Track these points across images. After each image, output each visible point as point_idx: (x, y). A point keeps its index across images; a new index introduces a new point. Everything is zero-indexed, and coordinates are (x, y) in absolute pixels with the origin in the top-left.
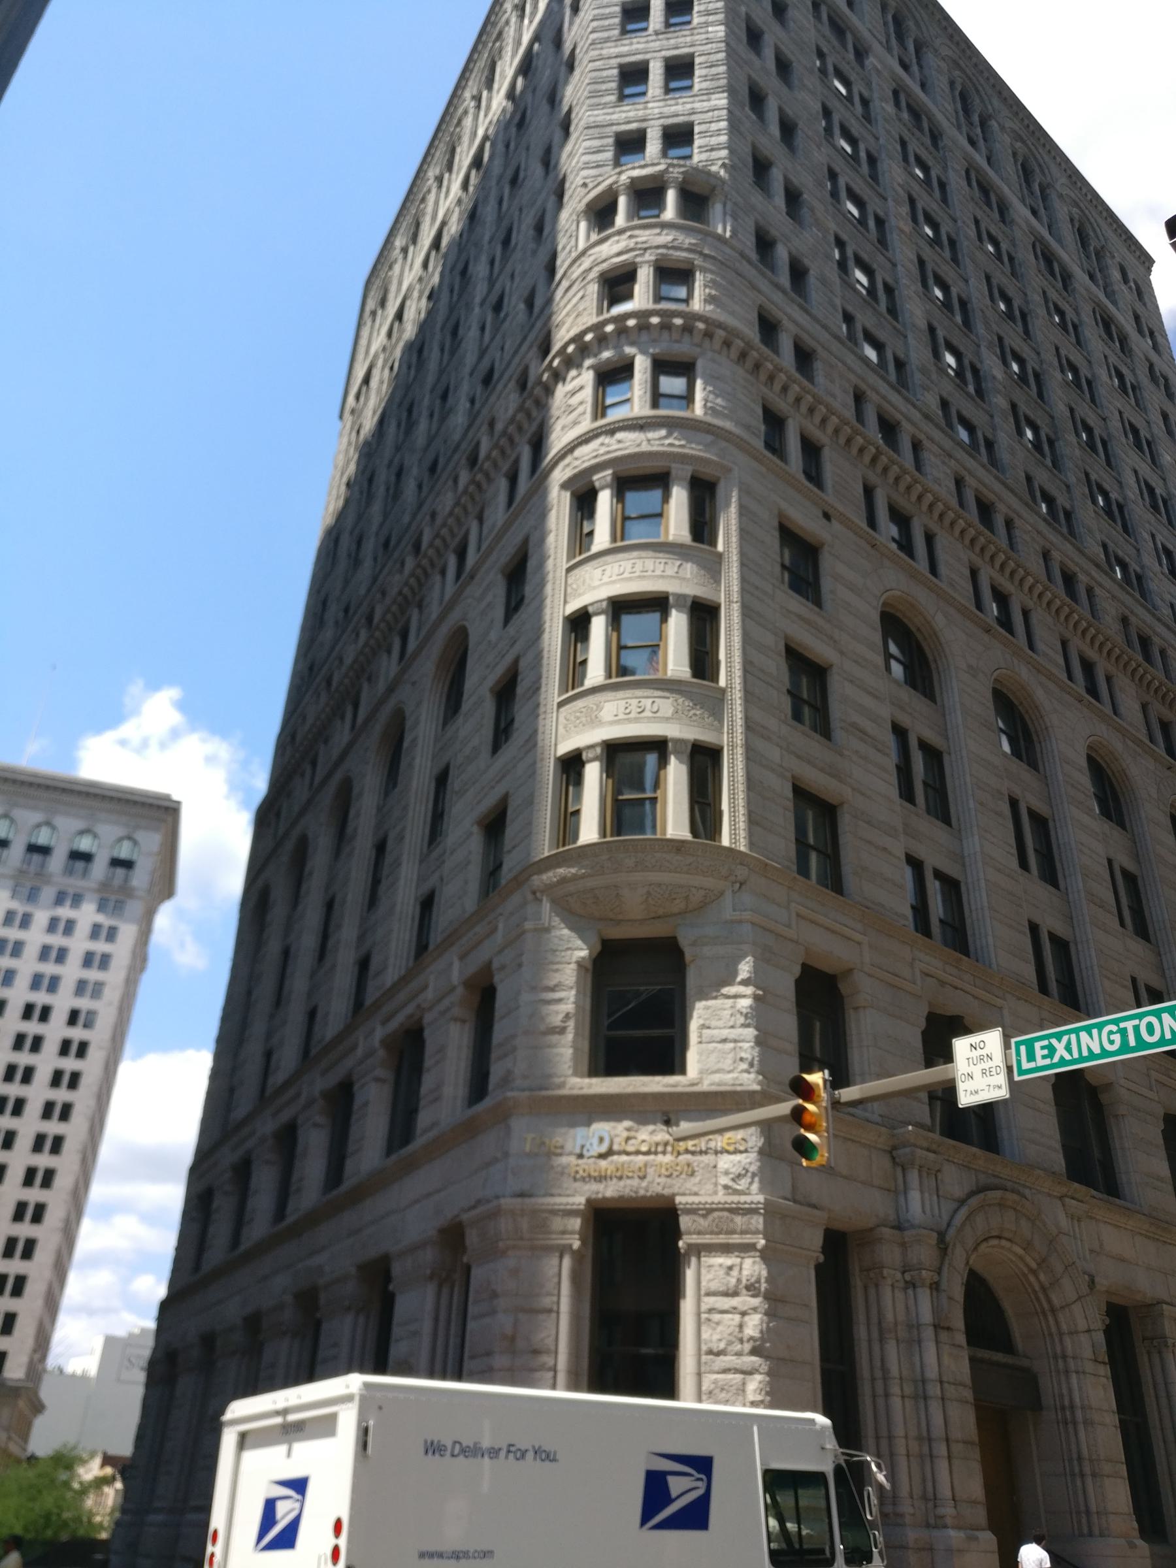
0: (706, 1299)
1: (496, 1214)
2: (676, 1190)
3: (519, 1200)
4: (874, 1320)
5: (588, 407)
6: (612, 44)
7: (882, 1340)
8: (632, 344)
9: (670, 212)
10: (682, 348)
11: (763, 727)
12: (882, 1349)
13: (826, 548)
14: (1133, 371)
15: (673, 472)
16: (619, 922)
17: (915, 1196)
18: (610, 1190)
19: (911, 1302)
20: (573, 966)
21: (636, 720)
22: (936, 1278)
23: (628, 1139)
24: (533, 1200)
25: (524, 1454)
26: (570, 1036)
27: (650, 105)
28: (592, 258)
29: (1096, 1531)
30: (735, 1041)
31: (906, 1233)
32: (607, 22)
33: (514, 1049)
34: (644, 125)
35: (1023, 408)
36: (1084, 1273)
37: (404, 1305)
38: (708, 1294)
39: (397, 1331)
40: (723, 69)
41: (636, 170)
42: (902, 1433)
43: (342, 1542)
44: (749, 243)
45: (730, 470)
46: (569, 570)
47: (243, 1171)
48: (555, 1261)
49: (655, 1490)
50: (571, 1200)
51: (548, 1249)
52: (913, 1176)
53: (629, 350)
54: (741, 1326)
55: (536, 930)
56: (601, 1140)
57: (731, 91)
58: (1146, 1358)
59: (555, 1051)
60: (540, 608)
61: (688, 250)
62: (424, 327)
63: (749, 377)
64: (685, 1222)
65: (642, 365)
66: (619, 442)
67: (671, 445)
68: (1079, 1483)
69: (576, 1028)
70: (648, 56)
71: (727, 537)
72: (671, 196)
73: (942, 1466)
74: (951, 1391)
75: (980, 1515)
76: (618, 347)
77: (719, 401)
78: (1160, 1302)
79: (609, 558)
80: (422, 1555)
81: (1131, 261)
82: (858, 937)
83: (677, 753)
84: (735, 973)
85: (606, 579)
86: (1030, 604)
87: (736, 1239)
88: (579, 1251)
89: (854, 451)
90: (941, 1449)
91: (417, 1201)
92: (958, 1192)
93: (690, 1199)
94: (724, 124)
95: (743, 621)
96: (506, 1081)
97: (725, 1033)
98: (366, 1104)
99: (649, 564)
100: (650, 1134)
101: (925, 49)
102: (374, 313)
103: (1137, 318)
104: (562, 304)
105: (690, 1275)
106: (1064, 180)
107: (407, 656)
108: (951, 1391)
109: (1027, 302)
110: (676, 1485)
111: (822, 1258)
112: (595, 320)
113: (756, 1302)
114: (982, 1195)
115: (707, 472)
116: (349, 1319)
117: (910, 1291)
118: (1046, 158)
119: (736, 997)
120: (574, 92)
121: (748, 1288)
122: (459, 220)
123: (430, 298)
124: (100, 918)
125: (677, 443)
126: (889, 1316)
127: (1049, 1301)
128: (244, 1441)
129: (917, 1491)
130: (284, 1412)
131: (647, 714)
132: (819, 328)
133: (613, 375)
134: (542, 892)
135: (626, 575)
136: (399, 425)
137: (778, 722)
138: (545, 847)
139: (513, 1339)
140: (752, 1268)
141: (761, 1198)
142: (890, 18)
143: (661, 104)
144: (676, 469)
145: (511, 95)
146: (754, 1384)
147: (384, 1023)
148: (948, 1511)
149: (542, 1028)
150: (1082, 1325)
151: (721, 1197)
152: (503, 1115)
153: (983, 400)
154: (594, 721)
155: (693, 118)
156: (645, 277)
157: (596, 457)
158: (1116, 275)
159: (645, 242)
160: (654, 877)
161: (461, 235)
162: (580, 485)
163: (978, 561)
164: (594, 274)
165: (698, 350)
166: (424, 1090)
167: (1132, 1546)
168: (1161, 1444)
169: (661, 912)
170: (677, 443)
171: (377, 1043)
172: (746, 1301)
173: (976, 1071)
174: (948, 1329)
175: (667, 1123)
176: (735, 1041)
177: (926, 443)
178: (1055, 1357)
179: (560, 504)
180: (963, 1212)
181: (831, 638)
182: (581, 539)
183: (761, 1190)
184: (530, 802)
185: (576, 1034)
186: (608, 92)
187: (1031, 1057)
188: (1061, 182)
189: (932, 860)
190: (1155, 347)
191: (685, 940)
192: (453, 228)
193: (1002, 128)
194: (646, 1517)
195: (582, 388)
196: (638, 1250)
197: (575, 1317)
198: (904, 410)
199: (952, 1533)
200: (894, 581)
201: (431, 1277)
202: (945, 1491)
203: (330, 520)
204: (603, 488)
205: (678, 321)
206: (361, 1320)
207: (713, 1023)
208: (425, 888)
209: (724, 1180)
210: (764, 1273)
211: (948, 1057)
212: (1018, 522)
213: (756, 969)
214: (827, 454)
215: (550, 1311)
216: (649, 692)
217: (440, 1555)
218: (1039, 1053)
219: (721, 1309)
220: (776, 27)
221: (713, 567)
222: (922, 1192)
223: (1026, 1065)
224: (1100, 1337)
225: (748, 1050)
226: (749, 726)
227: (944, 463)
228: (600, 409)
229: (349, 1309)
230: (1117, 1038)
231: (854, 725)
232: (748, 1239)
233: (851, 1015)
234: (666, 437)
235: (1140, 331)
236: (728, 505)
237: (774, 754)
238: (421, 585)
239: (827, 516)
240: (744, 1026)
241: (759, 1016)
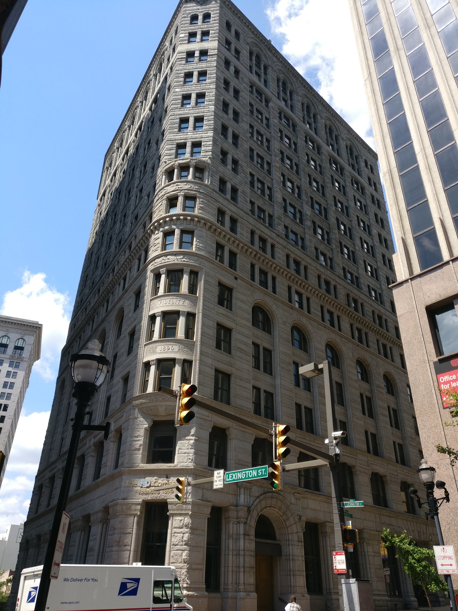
0: (174, 529)
1: (117, 504)
3: (123, 500)
5: (160, 245)
6: (178, 110)
7: (228, 539)
8: (174, 225)
9: (190, 177)
10: (190, 227)
11: (206, 353)
12: (228, 541)
13: (235, 289)
14: (365, 200)
15: (184, 270)
16: (158, 416)
17: (242, 496)
18: (149, 497)
19: (238, 527)
20: (143, 430)
21: (166, 353)
22: (246, 521)
23: (155, 482)
24: (127, 500)
25: (89, 580)
26: (141, 451)
27: (188, 134)
28: (165, 191)
29: (292, 592)
30: (188, 453)
31: (238, 507)
32: (177, 102)
33: (125, 455)
34: (186, 141)
35: (318, 223)
36: (298, 515)
37: (93, 529)
38: (174, 528)
39: (91, 538)
40: (212, 122)
41: (181, 161)
42: (231, 565)
44: (217, 184)
45: (202, 268)
46: (151, 300)
47: (52, 479)
48: (132, 518)
49: (123, 587)
50: (138, 500)
51: (131, 515)
52: (242, 490)
53: (174, 227)
54: (183, 537)
55: (133, 418)
56: (148, 482)
57: (215, 130)
58: (321, 539)
59: (137, 456)
60: (142, 312)
61: (195, 191)
62: (121, 184)
63: (212, 235)
64: (170, 507)
65: (177, 232)
66: (168, 259)
67: (184, 261)
68: (289, 578)
69: (143, 449)
70: (189, 115)
71: (200, 292)
72: (191, 170)
73: (242, 574)
74: (247, 553)
75: (253, 588)
76: (170, 225)
77: (201, 245)
79: (163, 298)
80: (62, 603)
81: (369, 157)
85: (161, 305)
86: (310, 296)
87: (183, 512)
88: (140, 515)
89: (248, 253)
90: (242, 570)
91: (99, 497)
92: (257, 494)
93: (171, 500)
94: (211, 143)
95: (202, 319)
96: (122, 464)
97: (186, 451)
98: (88, 463)
99: (175, 300)
101: (294, 93)
102: (107, 168)
103: (369, 179)
104: (156, 205)
105: (170, 522)
106: (346, 132)
107: (108, 311)
108: (247, 553)
109: (324, 182)
110: (129, 585)
111: (210, 517)
112: (164, 215)
113: (187, 530)
114: (265, 495)
115: (195, 269)
116: (79, 533)
117: (238, 524)
118: (339, 125)
119: (190, 440)
120: (166, 124)
121: (185, 526)
122: (133, 148)
123: (124, 173)
124: (10, 369)
125: (186, 260)
126: (231, 532)
127: (286, 524)
128: (25, 578)
129: (234, 582)
130: (34, 572)
131: (170, 350)
132: (240, 210)
133: (168, 234)
135: (167, 304)
136: (112, 219)
137: (212, 351)
138: (137, 392)
139: (119, 542)
140: (187, 520)
141: (191, 500)
142: (281, 84)
143: (192, 133)
144: (185, 268)
145: (150, 109)
147: (94, 438)
148: (242, 587)
149: (133, 449)
150: (295, 531)
152: (120, 475)
153: (302, 224)
154: (154, 352)
155: (202, 139)
156: (180, 199)
157: (161, 263)
158: (363, 164)
159: (181, 188)
161: (134, 154)
162: (156, 272)
163: (291, 284)
164: (165, 197)
165: (195, 227)
166: (103, 462)
167: (303, 596)
168: (323, 565)
169: (170, 413)
170: (186, 260)
171: (92, 445)
174: (248, 535)
176: (188, 453)
177: (277, 245)
178: (286, 541)
179: (150, 277)
180: (258, 500)
181: (233, 320)
184: (134, 376)
185: (143, 451)
186: (175, 128)
187: (228, 478)
188: (344, 134)
189: (263, 387)
190: (376, 190)
192: (131, 151)
193: (321, 118)
195: (159, 238)
196: (156, 514)
197: (137, 534)
198: (269, 234)
199: (242, 593)
200: (259, 296)
201: (100, 522)
202: (242, 581)
203: (90, 246)
204: (163, 274)
205: (189, 218)
206: (83, 533)
207: (182, 448)
208: (108, 394)
210: (190, 522)
211: (212, 475)
212: (309, 267)
213: (196, 431)
215: (130, 533)
216: (171, 343)
217: (66, 603)
218: (230, 477)
219: (178, 532)
220: (235, 101)
221: (194, 302)
222: (244, 495)
223: (227, 480)
224: (301, 535)
225: (191, 456)
226: (201, 353)
227: (282, 251)
228: (164, 246)
229: (79, 530)
230: (244, 475)
231: (239, 348)
232: (187, 512)
233: (229, 441)
234: (182, 258)
235: (370, 184)
236: (201, 281)
237: (209, 361)
238: (113, 287)
239: (236, 278)
241: (196, 446)
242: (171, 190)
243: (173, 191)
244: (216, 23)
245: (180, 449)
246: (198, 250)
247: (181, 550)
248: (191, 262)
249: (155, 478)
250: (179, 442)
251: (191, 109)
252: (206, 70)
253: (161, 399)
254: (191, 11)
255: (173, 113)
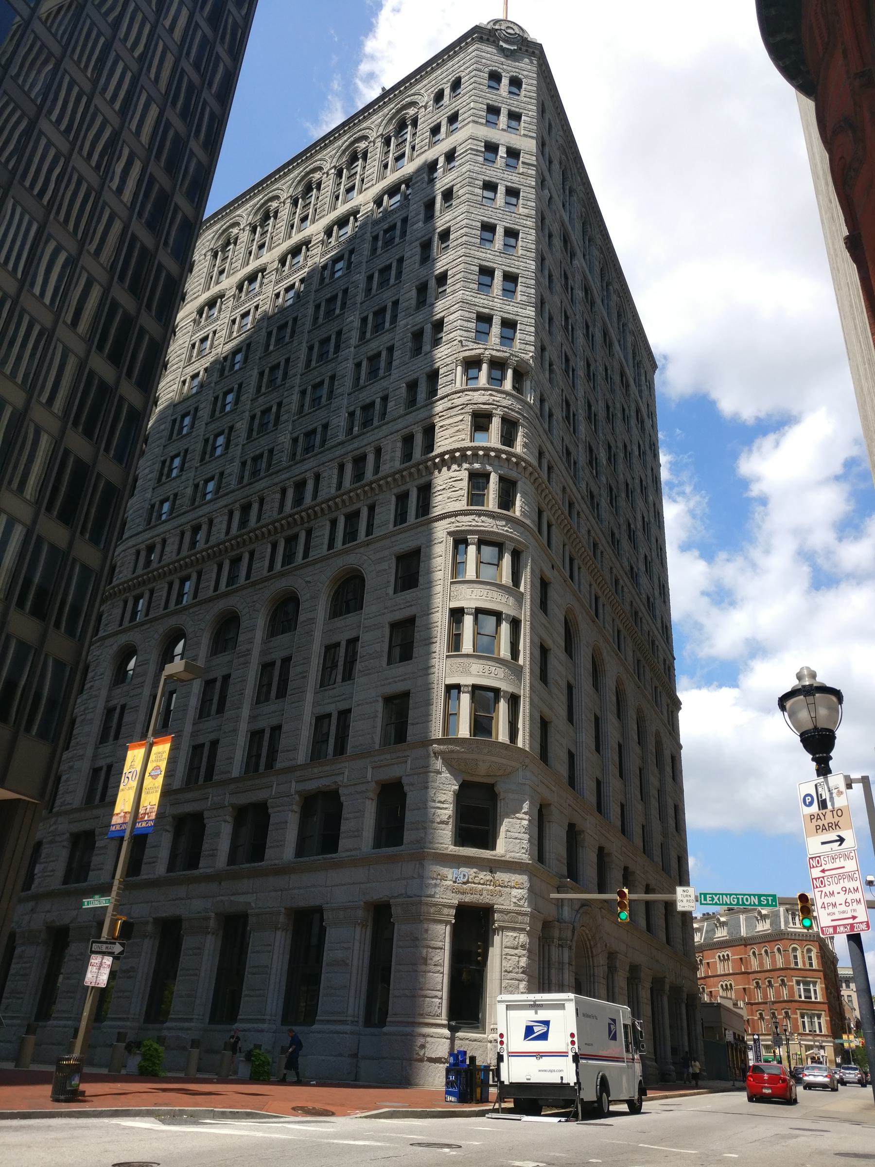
2: (494, 902)
4: (547, 960)
8: (490, 465)
18: (467, 899)
21: (488, 677)
28: (468, 398)
34: (492, 312)
43: (575, 1039)
53: (489, 468)
67: (507, 531)
78: (617, 952)
82: (553, 788)
83: (504, 697)
84: (521, 808)
87: (518, 926)
99: (495, 595)
100: (484, 876)
113: (525, 952)
119: (521, 819)
121: (521, 946)
127: (592, 952)
131: (492, 675)
134: (439, 754)
140: (523, 938)
146: (523, 985)
151: (512, 907)
154: (469, 673)
155: (518, 318)
160: (494, 759)
172: (520, 951)
173: (685, 899)
175: (491, 872)
182: (457, 566)
183: (529, 906)
191: (500, 788)
194: (526, 1037)
204: (472, 544)
207: (512, 830)
209: (515, 900)
214: (554, 528)
218: (708, 899)
225: (526, 844)
240: (524, 833)
242: (480, 401)
243: (484, 404)
244: (531, 104)
245: (507, 831)
246: (524, 517)
247: (516, 980)
248: (516, 535)
249: (475, 870)
250: (506, 820)
251: (498, 254)
252: (519, 190)
253: (486, 751)
254: (494, 64)
255: (468, 251)
